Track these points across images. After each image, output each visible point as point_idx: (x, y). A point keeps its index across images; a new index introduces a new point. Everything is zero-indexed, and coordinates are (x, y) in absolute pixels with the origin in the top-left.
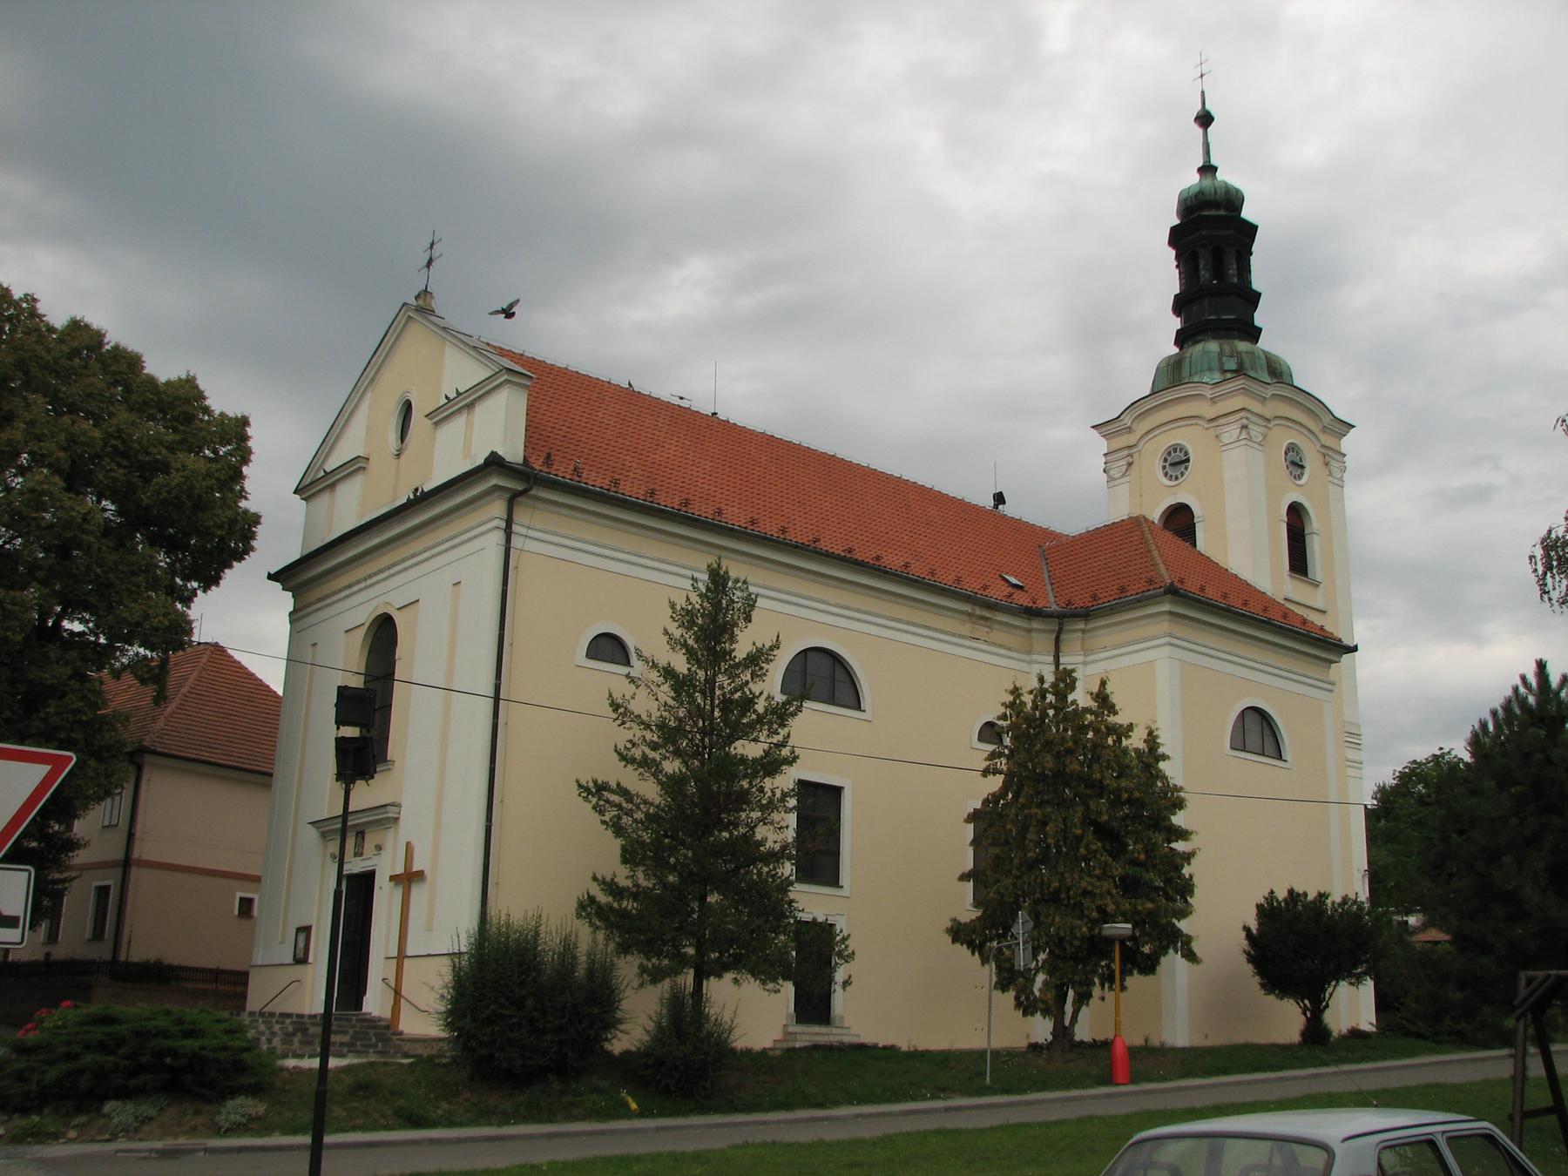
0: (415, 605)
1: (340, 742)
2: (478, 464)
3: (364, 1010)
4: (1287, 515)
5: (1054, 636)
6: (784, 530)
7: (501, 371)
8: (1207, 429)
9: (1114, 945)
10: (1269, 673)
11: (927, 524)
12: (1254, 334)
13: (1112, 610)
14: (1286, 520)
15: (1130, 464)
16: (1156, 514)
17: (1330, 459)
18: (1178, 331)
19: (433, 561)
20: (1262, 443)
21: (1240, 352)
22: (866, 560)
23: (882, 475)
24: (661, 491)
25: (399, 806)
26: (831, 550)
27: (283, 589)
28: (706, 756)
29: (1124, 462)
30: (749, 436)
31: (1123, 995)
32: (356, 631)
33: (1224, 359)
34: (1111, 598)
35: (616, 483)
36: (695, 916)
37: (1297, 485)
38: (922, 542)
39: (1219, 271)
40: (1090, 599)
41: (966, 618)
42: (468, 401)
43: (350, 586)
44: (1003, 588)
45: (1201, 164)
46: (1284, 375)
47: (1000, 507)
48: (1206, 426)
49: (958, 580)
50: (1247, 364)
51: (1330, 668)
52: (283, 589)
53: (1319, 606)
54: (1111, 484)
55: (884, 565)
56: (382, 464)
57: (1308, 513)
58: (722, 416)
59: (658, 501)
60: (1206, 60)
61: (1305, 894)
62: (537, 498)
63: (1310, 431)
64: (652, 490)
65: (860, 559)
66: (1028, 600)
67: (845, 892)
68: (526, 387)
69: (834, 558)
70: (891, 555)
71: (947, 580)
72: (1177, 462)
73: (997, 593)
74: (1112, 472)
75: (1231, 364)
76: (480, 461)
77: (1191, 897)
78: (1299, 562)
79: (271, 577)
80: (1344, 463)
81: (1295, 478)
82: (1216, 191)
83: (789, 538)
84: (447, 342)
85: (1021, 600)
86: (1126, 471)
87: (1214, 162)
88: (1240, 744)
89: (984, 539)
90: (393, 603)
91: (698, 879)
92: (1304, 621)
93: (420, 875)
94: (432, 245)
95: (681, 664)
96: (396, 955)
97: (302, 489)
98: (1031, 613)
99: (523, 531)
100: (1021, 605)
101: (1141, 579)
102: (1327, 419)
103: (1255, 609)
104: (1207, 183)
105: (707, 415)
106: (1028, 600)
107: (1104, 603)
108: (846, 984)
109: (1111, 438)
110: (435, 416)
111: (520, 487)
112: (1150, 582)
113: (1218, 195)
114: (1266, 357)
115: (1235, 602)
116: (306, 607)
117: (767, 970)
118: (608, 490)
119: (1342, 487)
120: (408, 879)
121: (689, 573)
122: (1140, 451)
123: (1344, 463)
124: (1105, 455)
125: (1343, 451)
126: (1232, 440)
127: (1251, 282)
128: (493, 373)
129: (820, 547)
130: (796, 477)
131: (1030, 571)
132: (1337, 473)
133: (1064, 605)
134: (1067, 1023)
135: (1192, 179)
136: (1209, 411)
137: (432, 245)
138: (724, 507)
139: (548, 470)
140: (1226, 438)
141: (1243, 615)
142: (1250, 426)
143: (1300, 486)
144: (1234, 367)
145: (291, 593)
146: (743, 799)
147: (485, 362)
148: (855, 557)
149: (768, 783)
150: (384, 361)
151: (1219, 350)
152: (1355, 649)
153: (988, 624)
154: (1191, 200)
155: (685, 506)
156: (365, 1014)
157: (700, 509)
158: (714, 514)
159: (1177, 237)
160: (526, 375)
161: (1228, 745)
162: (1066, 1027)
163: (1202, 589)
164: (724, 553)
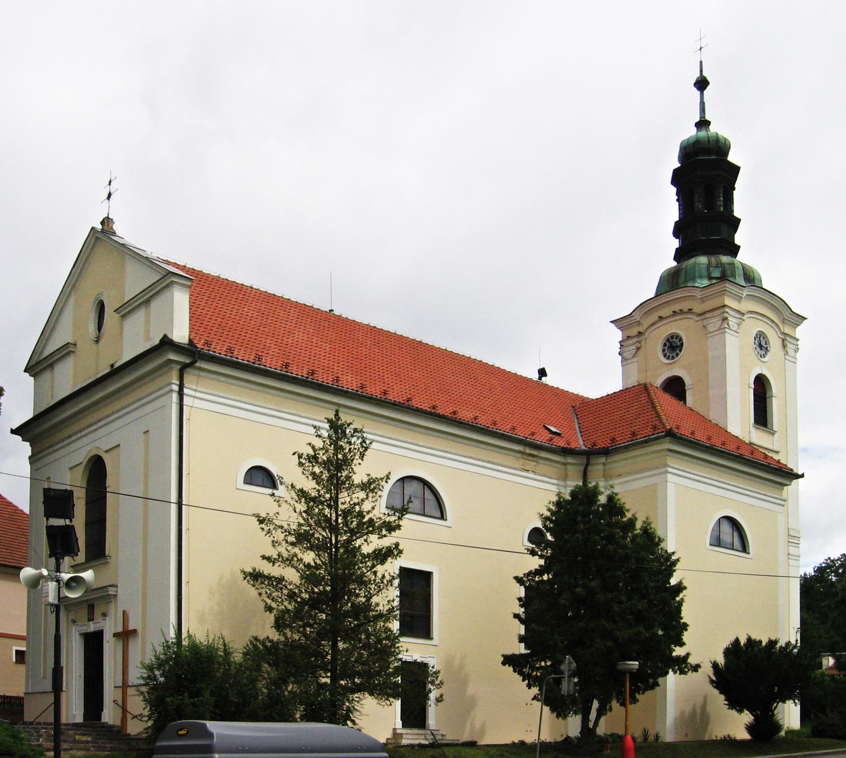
0: (115, 450)
1: (50, 529)
2: (155, 344)
3: (103, 721)
4: (754, 383)
5: (582, 468)
6: (385, 393)
7: (167, 274)
9: (625, 675)
10: (758, 499)
11: (490, 390)
12: (734, 250)
13: (626, 448)
14: (753, 387)
15: (638, 349)
16: (659, 382)
17: (787, 343)
18: (677, 249)
19: (127, 416)
20: (737, 331)
21: (724, 264)
22: (446, 414)
23: (457, 355)
24: (293, 364)
25: (117, 586)
26: (420, 407)
27: (23, 440)
28: (334, 550)
30: (358, 327)
31: (631, 707)
32: (76, 469)
33: (711, 269)
34: (625, 441)
35: (259, 358)
36: (329, 657)
37: (761, 361)
38: (486, 403)
39: (710, 203)
40: (609, 442)
41: (519, 455)
42: (146, 297)
43: (70, 437)
44: (547, 434)
45: (698, 120)
46: (756, 281)
47: (543, 379)
49: (514, 429)
50: (729, 272)
51: (783, 489)
52: (23, 440)
53: (775, 449)
54: (624, 363)
55: (459, 417)
56: (85, 347)
57: (769, 382)
58: (337, 312)
59: (292, 371)
60: (705, 36)
61: (760, 642)
62: (201, 369)
63: (773, 321)
64: (337, 377)
65: (441, 413)
66: (565, 443)
67: (435, 641)
68: (190, 287)
69: (435, 416)
70: (464, 411)
71: (505, 429)
72: (673, 346)
73: (542, 438)
74: (625, 354)
75: (716, 273)
76: (157, 342)
78: (762, 417)
79: (13, 432)
80: (798, 345)
81: (761, 357)
82: (709, 139)
83: (389, 398)
84: (127, 256)
85: (560, 443)
86: (636, 353)
87: (707, 118)
88: (717, 542)
89: (532, 401)
90: (102, 448)
91: (332, 632)
92: (766, 457)
93: (134, 632)
94: (110, 182)
95: (309, 486)
96: (121, 685)
97: (29, 368)
98: (566, 452)
99: (192, 393)
100: (559, 446)
101: (648, 426)
102: (787, 314)
103: (731, 447)
104: (703, 134)
105: (326, 312)
106: (565, 443)
107: (620, 444)
108: (439, 700)
109: (626, 329)
110: (122, 311)
111: (188, 361)
112: (655, 427)
114: (743, 267)
115: (717, 442)
116: (39, 453)
117: (383, 691)
118: (254, 363)
119: (795, 363)
120: (126, 635)
121: (311, 422)
122: (646, 339)
123: (798, 345)
125: (797, 337)
126: (716, 329)
127: (733, 211)
128: (162, 276)
129: (412, 404)
130: (393, 356)
131: (565, 423)
132: (791, 352)
133: (590, 446)
134: (591, 725)
135: (690, 132)
136: (698, 308)
137: (110, 182)
138: (339, 375)
139: (208, 348)
140: (711, 328)
141: (722, 452)
142: (729, 318)
143: (763, 362)
145: (28, 443)
146: (362, 582)
147: (154, 267)
148: (438, 412)
149: (380, 569)
152: (802, 476)
153: (535, 459)
154: (690, 147)
155: (312, 375)
156: (103, 723)
157: (321, 377)
158: (333, 381)
159: (677, 178)
160: (180, 275)
161: (708, 542)
162: (590, 728)
163: (693, 433)
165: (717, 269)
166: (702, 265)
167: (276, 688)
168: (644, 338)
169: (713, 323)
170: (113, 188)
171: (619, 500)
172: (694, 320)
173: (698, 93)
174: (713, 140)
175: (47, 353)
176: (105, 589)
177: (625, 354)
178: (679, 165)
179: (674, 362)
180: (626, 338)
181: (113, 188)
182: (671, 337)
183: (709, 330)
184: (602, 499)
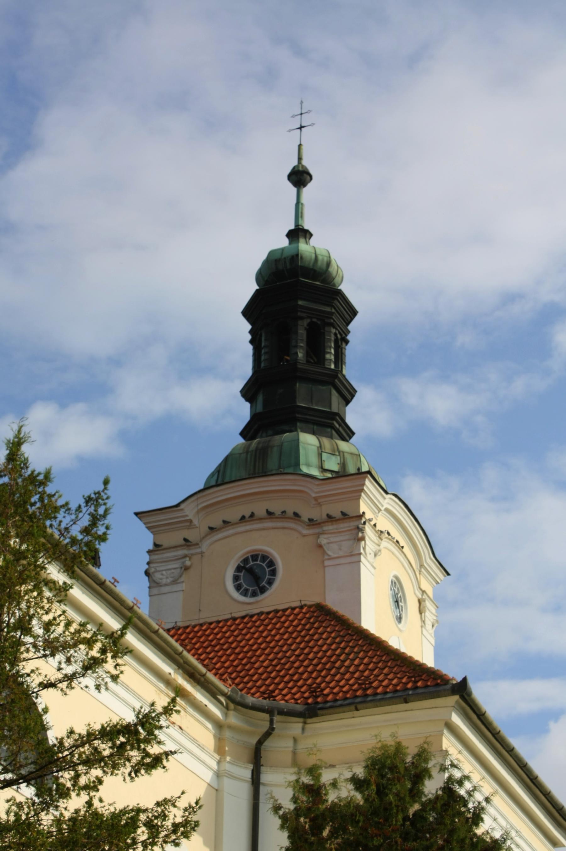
8: (304, 536)
21: (343, 452)
29: (177, 565)
48: (305, 532)
54: (155, 591)
113: (319, 263)
124: (149, 552)
126: (341, 554)
144: (336, 468)
151: (318, 444)
164: (500, 790)
165: (333, 458)
166: (310, 447)
167: (25, 558)
168: (199, 550)
171: (89, 521)
172: (300, 533)
173: (294, 190)
174: (323, 260)
177: (157, 576)
178: (257, 288)
179: (257, 602)
182: (252, 556)
183: (330, 553)
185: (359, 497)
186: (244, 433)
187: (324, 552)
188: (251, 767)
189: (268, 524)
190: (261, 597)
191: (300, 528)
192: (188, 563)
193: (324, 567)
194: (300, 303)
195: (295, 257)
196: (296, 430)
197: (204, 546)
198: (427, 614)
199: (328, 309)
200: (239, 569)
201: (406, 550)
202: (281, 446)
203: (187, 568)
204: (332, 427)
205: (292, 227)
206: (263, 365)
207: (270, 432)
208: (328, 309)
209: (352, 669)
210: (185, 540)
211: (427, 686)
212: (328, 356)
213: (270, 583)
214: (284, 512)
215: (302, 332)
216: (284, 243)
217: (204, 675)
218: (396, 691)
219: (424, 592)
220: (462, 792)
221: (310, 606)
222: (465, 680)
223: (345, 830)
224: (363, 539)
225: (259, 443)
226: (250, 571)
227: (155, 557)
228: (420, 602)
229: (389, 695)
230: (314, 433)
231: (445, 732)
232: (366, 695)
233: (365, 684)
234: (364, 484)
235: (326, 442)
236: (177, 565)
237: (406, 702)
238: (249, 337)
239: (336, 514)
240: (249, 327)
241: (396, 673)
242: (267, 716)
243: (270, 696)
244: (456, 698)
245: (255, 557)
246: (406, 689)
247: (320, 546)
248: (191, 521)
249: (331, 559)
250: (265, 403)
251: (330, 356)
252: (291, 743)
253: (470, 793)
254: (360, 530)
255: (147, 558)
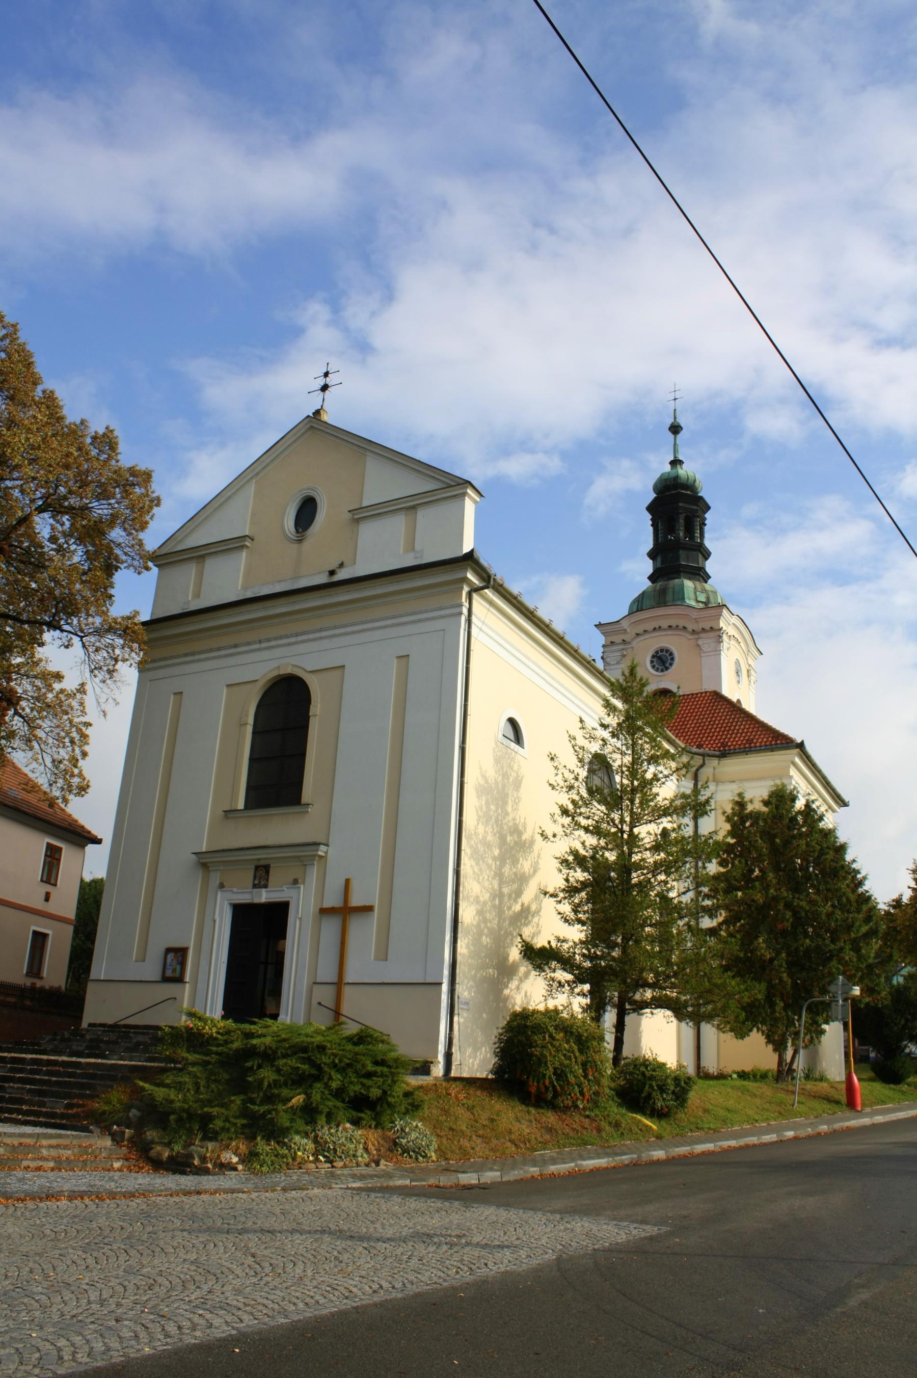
29: (619, 654)
77: (859, 873)
135: (667, 468)
144: (704, 600)
150: (245, 484)
169: (706, 642)
170: (330, 380)
173: (673, 436)
175: (191, 542)
176: (307, 852)
177: (608, 660)
179: (664, 675)
180: (609, 643)
181: (330, 380)
184: (800, 804)
185: (719, 619)
186: (650, 578)
187: (701, 649)
188: (693, 782)
189: (669, 632)
190: (666, 672)
191: (686, 635)
192: (625, 653)
193: (701, 657)
194: (680, 504)
195: (677, 477)
196: (680, 578)
197: (634, 644)
198: (752, 677)
199: (695, 507)
200: (653, 657)
201: (741, 644)
202: (674, 588)
203: (624, 656)
204: (700, 575)
205: (672, 458)
206: (660, 540)
207: (665, 578)
208: (695, 507)
209: (740, 731)
210: (623, 640)
211: (782, 744)
212: (696, 535)
213: (671, 664)
214: (677, 626)
215: (682, 521)
216: (667, 468)
217: (674, 741)
218: (766, 745)
219: (750, 665)
220: (814, 806)
221: (711, 692)
222: (802, 742)
223: (757, 823)
224: (722, 642)
225: (661, 585)
226: (660, 658)
227: (606, 649)
228: (748, 671)
229: (763, 748)
230: (690, 579)
231: (792, 766)
232: (751, 747)
233: (750, 741)
234: (722, 612)
235: (697, 583)
236: (619, 654)
237: (772, 751)
238: (651, 523)
239: (708, 628)
240: (651, 517)
241: (764, 735)
242: (701, 757)
243: (699, 747)
244: (798, 750)
245: (662, 650)
246: (772, 745)
247: (698, 645)
248: (625, 630)
249: (704, 652)
250: (663, 562)
251: (697, 535)
252: (712, 770)
253: (818, 808)
254: (720, 637)
255: (602, 650)
